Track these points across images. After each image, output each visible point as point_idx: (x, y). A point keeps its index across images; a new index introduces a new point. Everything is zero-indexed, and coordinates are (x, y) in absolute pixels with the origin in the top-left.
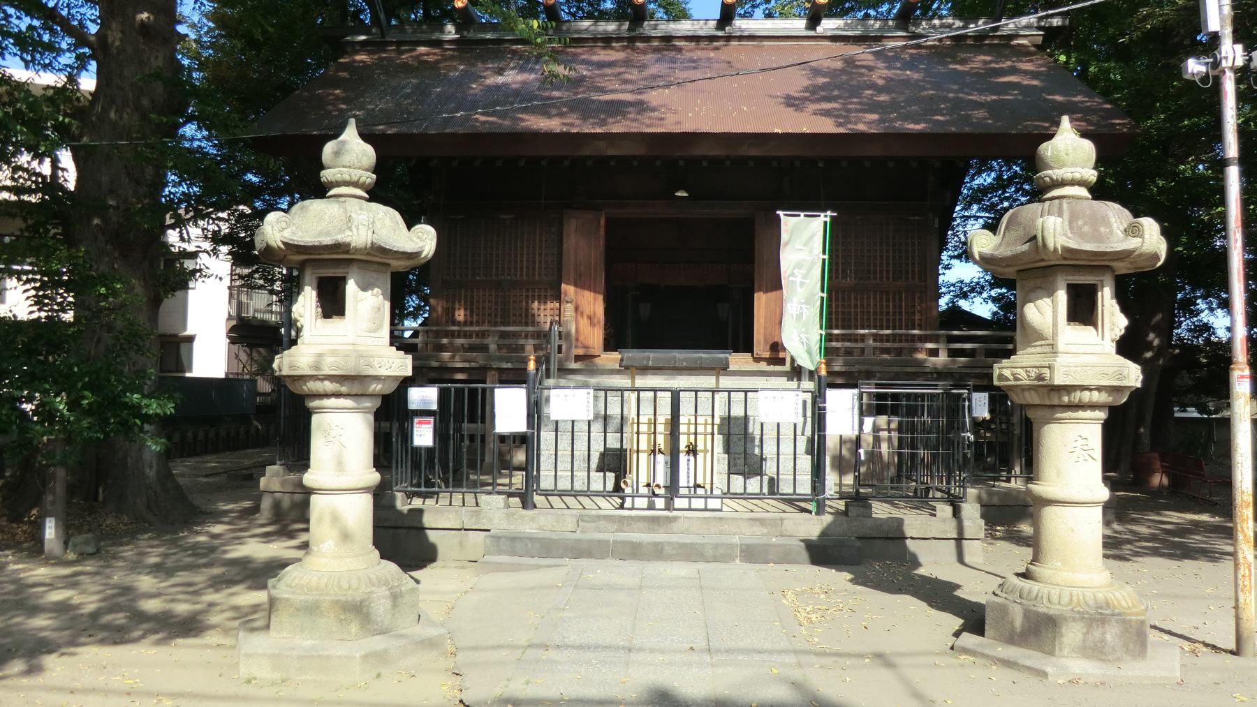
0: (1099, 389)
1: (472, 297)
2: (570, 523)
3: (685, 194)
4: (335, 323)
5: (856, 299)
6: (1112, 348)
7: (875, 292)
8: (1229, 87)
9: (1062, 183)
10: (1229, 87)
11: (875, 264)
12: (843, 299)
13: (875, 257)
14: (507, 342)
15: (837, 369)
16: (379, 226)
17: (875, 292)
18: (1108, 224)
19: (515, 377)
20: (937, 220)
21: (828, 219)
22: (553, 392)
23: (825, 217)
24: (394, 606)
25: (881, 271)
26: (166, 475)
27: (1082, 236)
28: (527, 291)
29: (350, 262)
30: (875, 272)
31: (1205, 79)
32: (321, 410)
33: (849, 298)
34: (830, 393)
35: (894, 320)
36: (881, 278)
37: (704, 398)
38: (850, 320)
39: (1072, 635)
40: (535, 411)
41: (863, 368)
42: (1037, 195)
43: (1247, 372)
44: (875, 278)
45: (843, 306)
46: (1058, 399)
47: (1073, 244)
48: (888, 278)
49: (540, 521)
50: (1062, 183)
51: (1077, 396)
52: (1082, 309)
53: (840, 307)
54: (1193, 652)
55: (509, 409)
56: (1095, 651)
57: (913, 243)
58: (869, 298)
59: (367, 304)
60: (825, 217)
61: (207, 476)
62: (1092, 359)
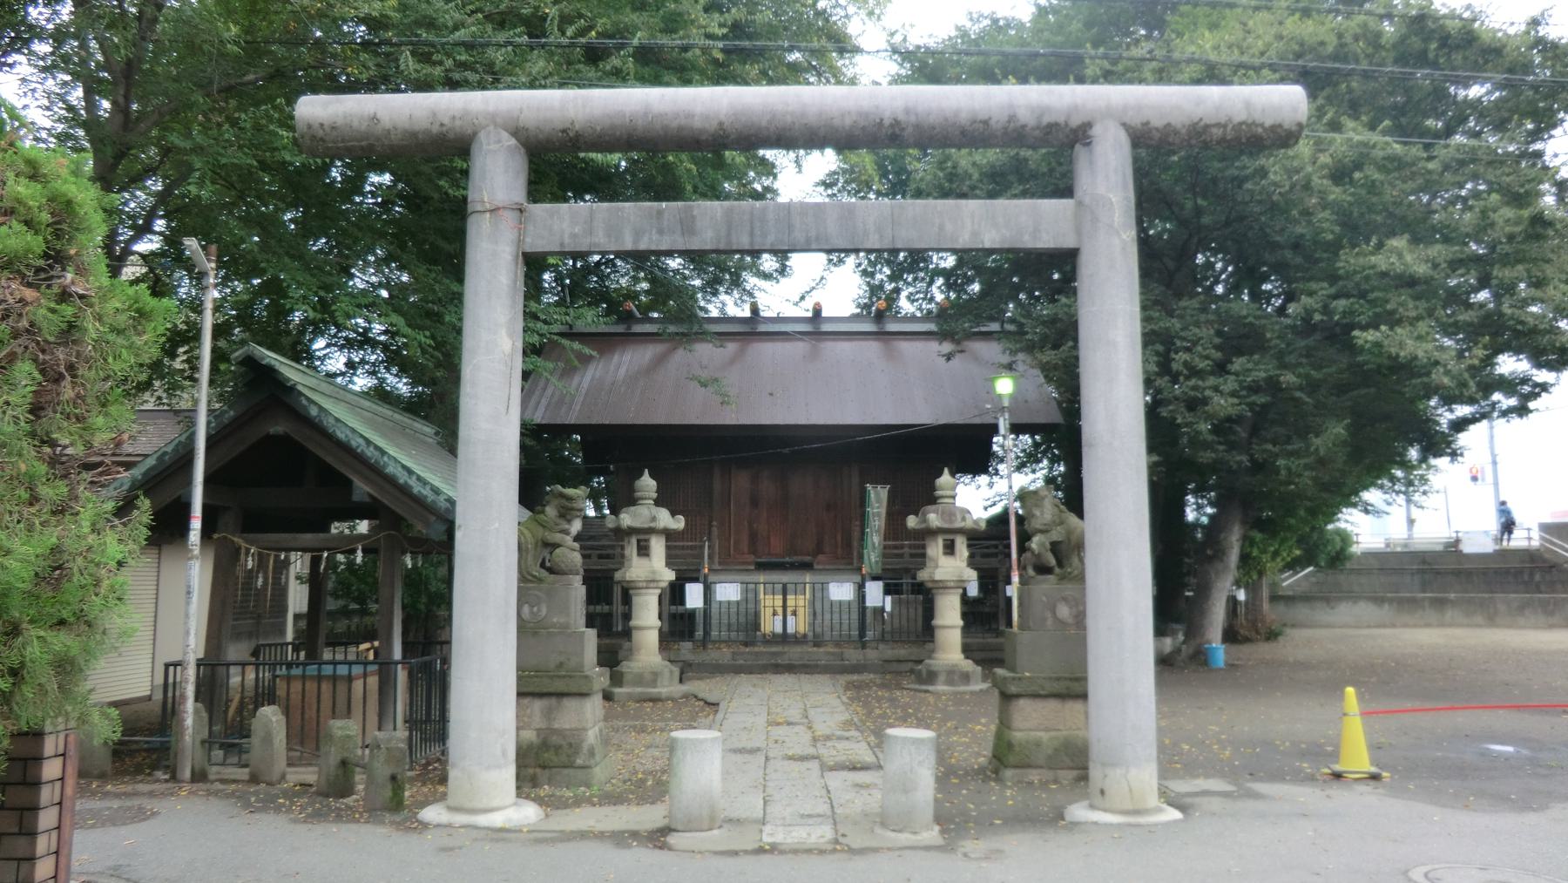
1: (785, 607)
2: (729, 656)
4: (644, 561)
39: (942, 678)
46: (943, 586)
52: (950, 549)
56: (950, 682)
59: (658, 546)
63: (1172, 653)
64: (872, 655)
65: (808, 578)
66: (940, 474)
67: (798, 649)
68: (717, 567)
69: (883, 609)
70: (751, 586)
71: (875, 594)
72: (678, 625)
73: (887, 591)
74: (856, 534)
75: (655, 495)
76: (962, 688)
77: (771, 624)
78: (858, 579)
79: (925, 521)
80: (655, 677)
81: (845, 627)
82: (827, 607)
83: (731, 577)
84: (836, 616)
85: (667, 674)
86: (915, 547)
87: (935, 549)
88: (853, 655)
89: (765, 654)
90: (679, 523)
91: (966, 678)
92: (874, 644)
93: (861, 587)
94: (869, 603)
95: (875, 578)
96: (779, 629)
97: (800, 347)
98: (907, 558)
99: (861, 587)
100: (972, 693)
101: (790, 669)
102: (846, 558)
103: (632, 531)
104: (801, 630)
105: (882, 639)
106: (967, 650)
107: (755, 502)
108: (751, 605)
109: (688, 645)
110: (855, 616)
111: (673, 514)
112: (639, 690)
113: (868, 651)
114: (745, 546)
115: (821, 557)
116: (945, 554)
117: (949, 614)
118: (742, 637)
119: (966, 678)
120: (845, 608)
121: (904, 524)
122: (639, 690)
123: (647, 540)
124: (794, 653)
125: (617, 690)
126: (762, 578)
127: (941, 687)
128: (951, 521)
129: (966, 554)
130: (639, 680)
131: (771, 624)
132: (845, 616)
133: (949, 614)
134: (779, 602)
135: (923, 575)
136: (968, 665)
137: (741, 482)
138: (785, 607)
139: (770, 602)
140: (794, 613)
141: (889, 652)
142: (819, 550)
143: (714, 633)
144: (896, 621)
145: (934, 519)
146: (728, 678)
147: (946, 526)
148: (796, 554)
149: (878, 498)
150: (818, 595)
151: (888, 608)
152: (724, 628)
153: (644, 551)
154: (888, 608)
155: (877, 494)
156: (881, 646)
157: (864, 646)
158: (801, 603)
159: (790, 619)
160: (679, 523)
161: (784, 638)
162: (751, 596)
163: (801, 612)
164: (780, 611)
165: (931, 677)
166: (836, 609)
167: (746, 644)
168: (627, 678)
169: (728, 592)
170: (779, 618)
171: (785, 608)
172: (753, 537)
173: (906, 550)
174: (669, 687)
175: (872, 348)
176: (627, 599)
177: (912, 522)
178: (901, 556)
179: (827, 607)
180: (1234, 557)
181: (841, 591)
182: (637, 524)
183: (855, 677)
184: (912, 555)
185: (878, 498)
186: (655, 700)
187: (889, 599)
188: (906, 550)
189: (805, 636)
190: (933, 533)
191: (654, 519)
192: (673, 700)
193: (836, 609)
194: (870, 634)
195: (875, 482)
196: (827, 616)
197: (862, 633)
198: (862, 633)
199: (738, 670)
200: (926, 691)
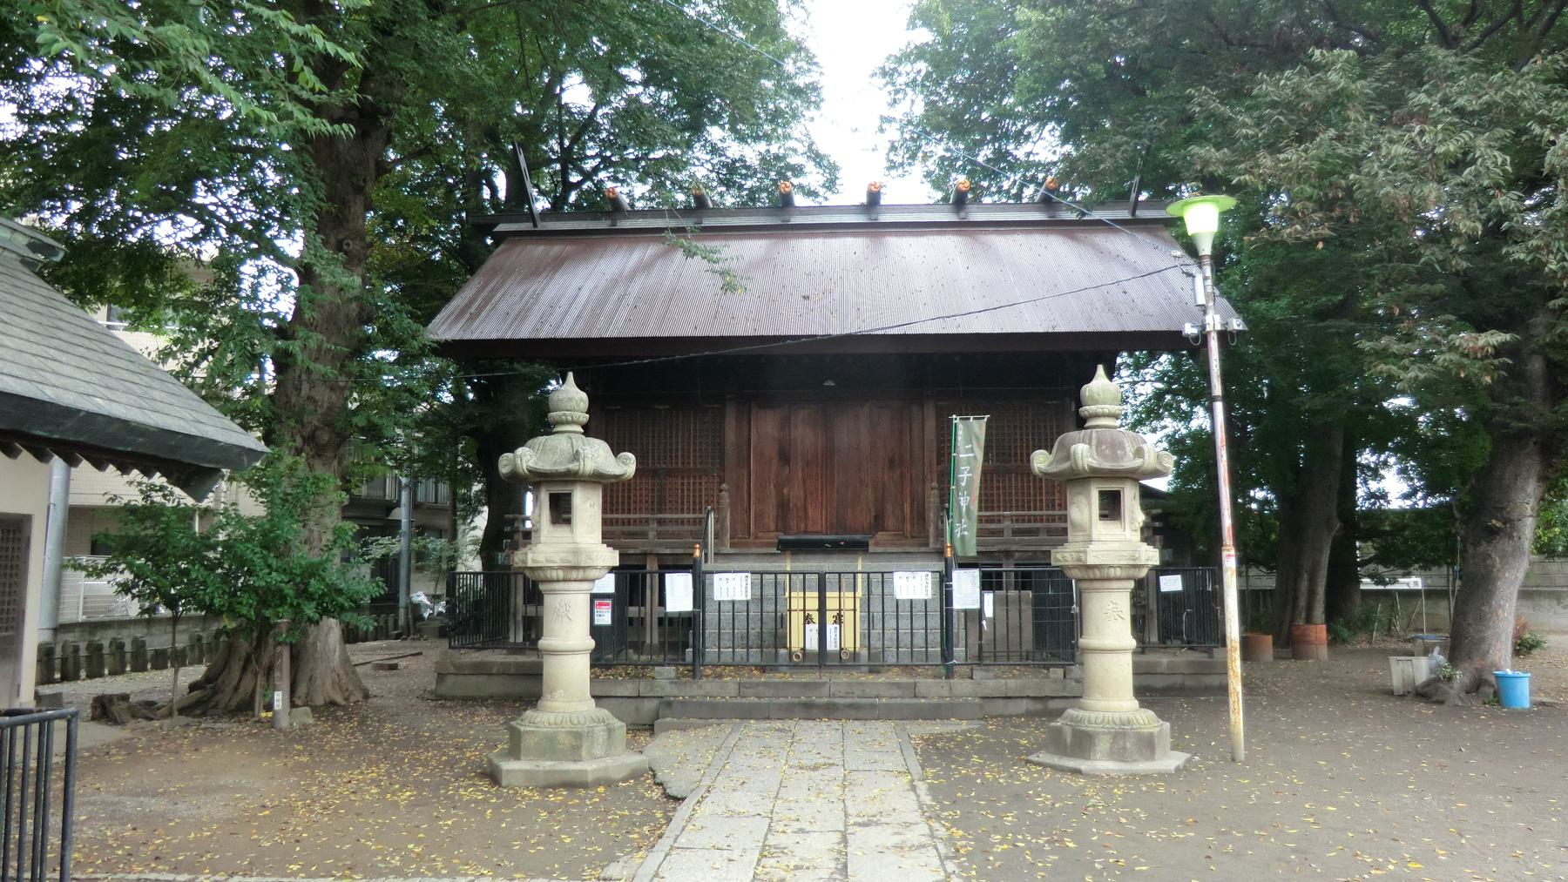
0: (1120, 567)
1: (822, 609)
2: (733, 689)
4: (562, 532)
6: (1137, 536)
8: (1214, 344)
9: (1096, 416)
10: (1214, 344)
14: (663, 528)
16: (598, 456)
18: (1123, 449)
24: (609, 737)
26: (346, 660)
27: (1104, 457)
31: (1196, 338)
32: (553, 592)
37: (20, 730)
39: (1103, 745)
40: (700, 592)
41: (1002, 548)
42: (1081, 423)
43: (1233, 552)
46: (1098, 576)
47: (1095, 464)
49: (706, 688)
50: (1096, 416)
51: (1105, 573)
52: (1111, 506)
56: (1118, 754)
59: (588, 506)
62: (1116, 546)
63: (1428, 684)
64: (962, 687)
65: (860, 564)
66: (1089, 378)
67: (842, 678)
68: (728, 550)
69: (980, 612)
70: (769, 578)
71: (967, 589)
72: (636, 638)
73: (988, 583)
74: (932, 499)
75: (585, 418)
76: (1143, 766)
77: (803, 637)
78: (940, 566)
79: (1068, 457)
80: (577, 742)
81: (919, 640)
82: (890, 608)
83: (734, 565)
84: (905, 624)
85: (600, 734)
86: (992, 533)
87: (1084, 508)
88: (932, 688)
89: (789, 685)
90: (626, 465)
91: (1147, 745)
92: (966, 670)
93: (944, 581)
94: (958, 604)
95: (965, 565)
96: (813, 645)
97: (854, 245)
98: (1008, 535)
99: (944, 581)
100: (1163, 776)
101: (830, 711)
102: (918, 533)
103: (538, 479)
104: (849, 645)
105: (980, 658)
106: (1145, 693)
107: (785, 457)
108: (769, 607)
109: (670, 671)
110: (935, 622)
111: (616, 451)
112: (547, 765)
113: (955, 681)
114: (770, 521)
115: (880, 535)
116: (1103, 517)
117: (1110, 624)
118: (755, 657)
119: (1147, 745)
120: (919, 612)
121: (1026, 471)
122: (547, 765)
123: (569, 496)
124: (838, 683)
125: (508, 766)
126: (788, 565)
127: (1101, 764)
128: (1116, 458)
129: (1141, 518)
130: (549, 747)
131: (803, 637)
132: (919, 623)
133: (1110, 624)
134: (813, 604)
135: (1062, 556)
136: (1147, 720)
137: (766, 426)
138: (822, 609)
139: (802, 601)
140: (839, 619)
141: (989, 681)
142: (878, 524)
143: (711, 650)
144: (1001, 630)
145: (1084, 452)
146: (727, 726)
147: (1107, 465)
148: (845, 532)
149: (970, 439)
150: (876, 590)
151: (989, 612)
152: (727, 641)
153: (561, 510)
154: (989, 612)
155: (968, 429)
156: (978, 674)
157: (950, 674)
158: (848, 604)
159: (832, 629)
160: (626, 465)
161: (822, 659)
162: (769, 592)
163: (848, 617)
164: (815, 616)
165: (1082, 743)
166: (905, 613)
167: (763, 669)
168: (527, 742)
169: (731, 586)
170: (813, 629)
171: (829, 609)
172: (783, 506)
173: (1007, 523)
174: (609, 758)
175: (949, 244)
176: (534, 595)
177: (1041, 461)
178: (1000, 532)
179: (890, 608)
180: (1528, 528)
181: (912, 584)
182: (546, 465)
183: (936, 728)
184: (1016, 532)
185: (970, 439)
186: (573, 785)
187: (989, 597)
188: (1007, 523)
189: (855, 655)
190: (1079, 479)
191: (576, 456)
192: (609, 783)
193: (905, 613)
194: (959, 651)
195: (964, 412)
196: (891, 623)
197: (947, 654)
198: (947, 654)
199: (746, 713)
200: (1076, 772)
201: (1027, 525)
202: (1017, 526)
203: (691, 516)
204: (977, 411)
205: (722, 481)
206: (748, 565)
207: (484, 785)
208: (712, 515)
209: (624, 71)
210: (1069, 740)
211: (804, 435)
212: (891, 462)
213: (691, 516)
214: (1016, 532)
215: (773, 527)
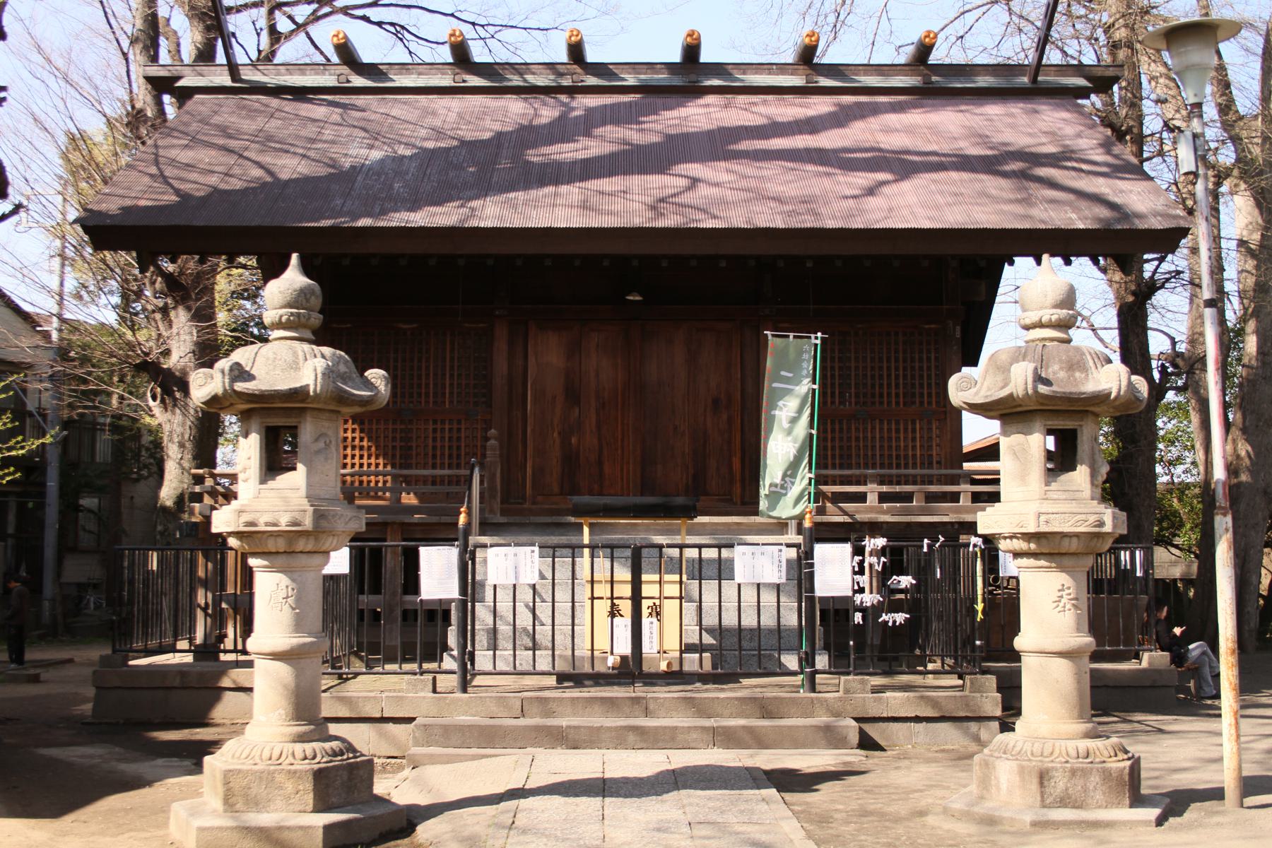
1: (636, 598)
3: (638, 298)
5: (857, 429)
7: (881, 422)
11: (881, 386)
12: (841, 430)
13: (881, 377)
15: (398, 642)
17: (881, 422)
19: (441, 534)
20: (958, 328)
21: (818, 342)
22: (491, 552)
23: (817, 338)
25: (889, 394)
28: (435, 422)
29: (303, 410)
30: (881, 395)
33: (849, 429)
34: (819, 549)
35: (906, 457)
36: (889, 403)
38: (850, 456)
44: (881, 403)
45: (841, 439)
48: (897, 403)
53: (833, 452)
54: (70, 61)
55: (437, 573)
57: (929, 359)
58: (873, 428)
60: (817, 338)
61: (70, 661)
107: (573, 394)
137: (548, 356)
138: (636, 598)
140: (657, 612)
164: (626, 607)
170: (623, 625)
201: (898, 489)
202: (885, 489)
203: (446, 472)
204: (803, 326)
205: (488, 425)
206: (539, 539)
207: (764, 804)
208: (477, 471)
209: (1147, 275)
210: (123, 767)
211: (601, 368)
212: (716, 402)
213: (446, 472)
214: (883, 498)
215: (556, 489)
